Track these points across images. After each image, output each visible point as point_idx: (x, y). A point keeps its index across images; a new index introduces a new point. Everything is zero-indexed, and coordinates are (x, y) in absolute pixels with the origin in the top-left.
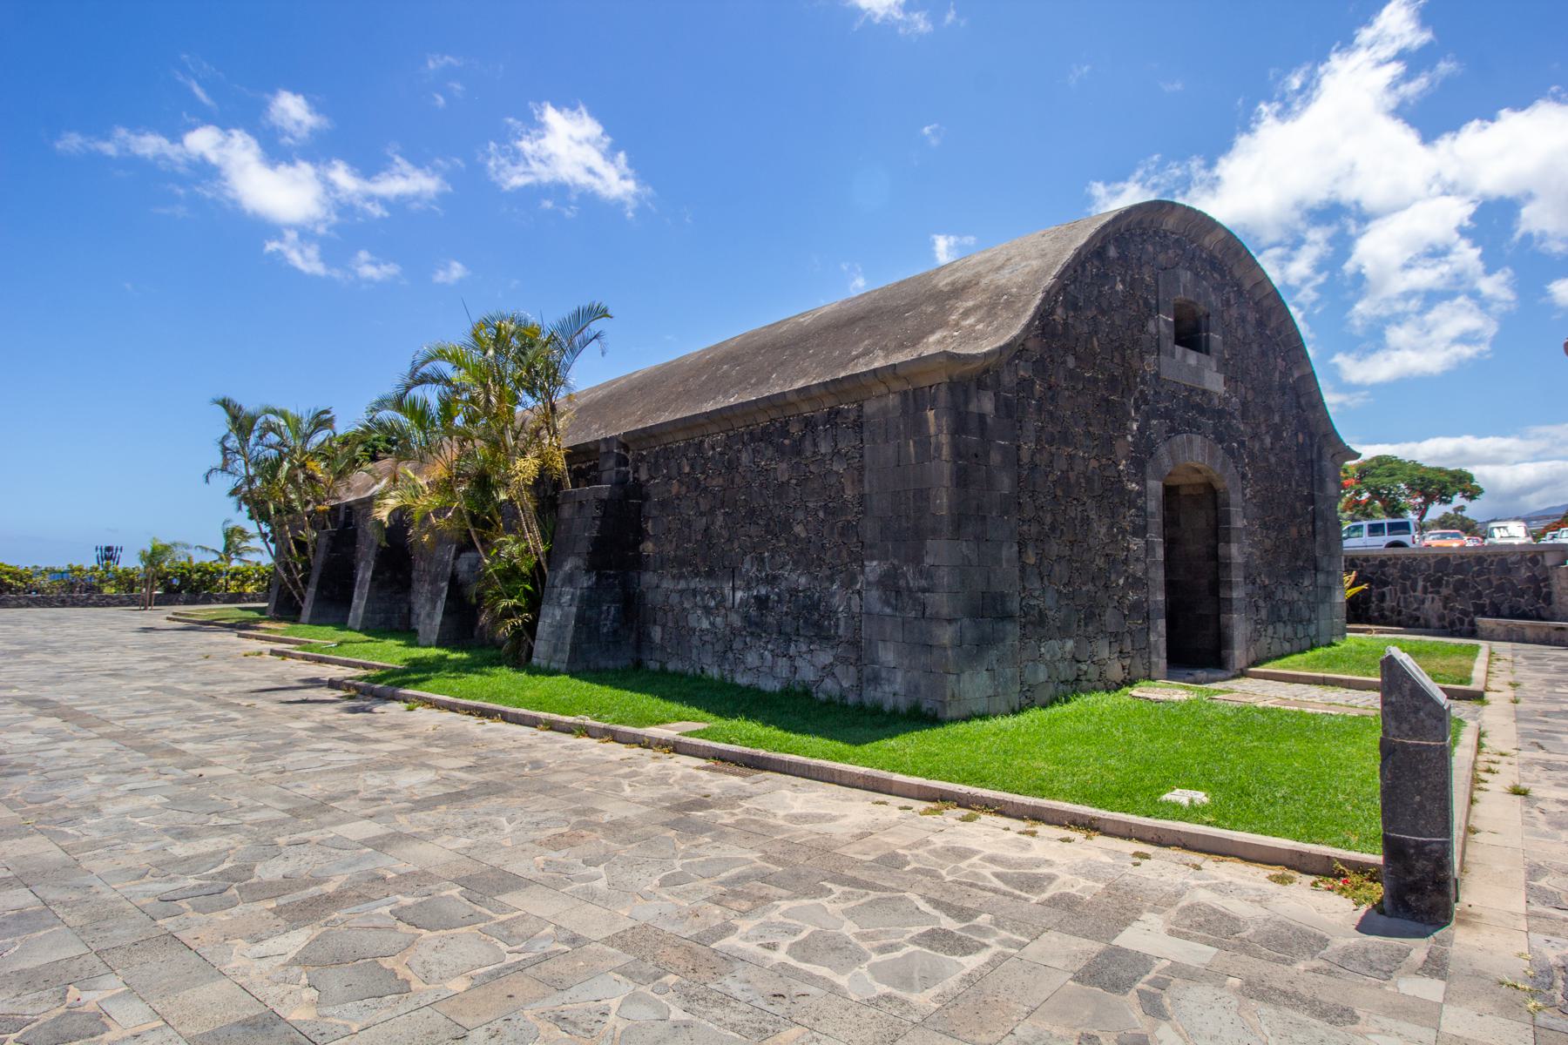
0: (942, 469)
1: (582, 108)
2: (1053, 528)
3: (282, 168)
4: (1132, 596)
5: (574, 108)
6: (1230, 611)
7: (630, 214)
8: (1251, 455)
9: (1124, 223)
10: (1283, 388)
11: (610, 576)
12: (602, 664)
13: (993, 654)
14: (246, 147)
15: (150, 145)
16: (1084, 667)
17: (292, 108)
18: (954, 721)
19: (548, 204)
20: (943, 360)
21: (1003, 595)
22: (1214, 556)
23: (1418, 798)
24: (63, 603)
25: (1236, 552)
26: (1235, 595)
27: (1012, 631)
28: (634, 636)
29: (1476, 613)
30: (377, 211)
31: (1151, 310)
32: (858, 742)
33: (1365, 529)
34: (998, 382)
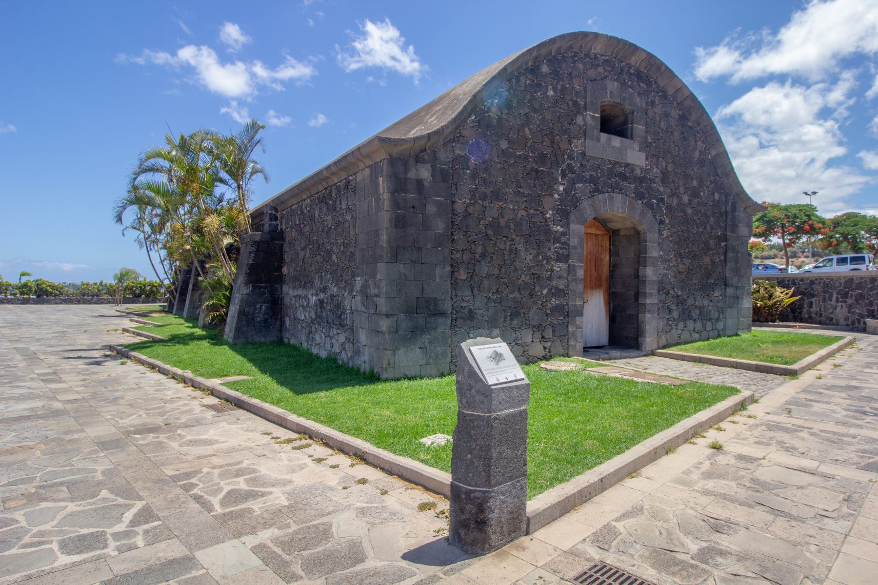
0: (385, 217)
1: (387, 20)
2: (483, 256)
3: (228, 66)
4: (554, 301)
5: (382, 21)
6: (645, 312)
7: (416, 82)
8: (670, 208)
9: (554, 48)
10: (702, 163)
11: (261, 287)
12: (257, 339)
13: (426, 338)
14: (210, 55)
15: (162, 57)
17: (232, 32)
18: (386, 380)
19: (370, 79)
20: (377, 142)
22: (637, 276)
23: (469, 456)
24: (79, 302)
25: (650, 273)
26: (648, 301)
27: (443, 325)
28: (278, 323)
29: (868, 317)
30: (279, 88)
31: (578, 109)
32: (298, 392)
33: (835, 261)
34: (435, 158)
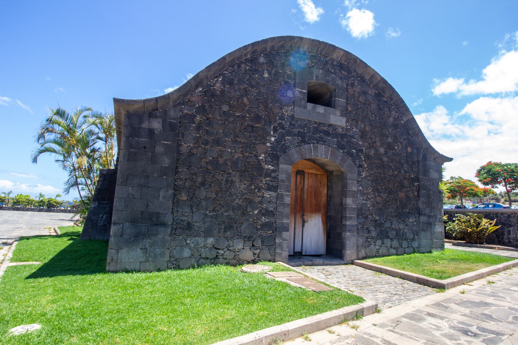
6: (345, 231)
10: (395, 126)
11: (104, 204)
13: (147, 242)
16: (221, 252)
21: (158, 214)
